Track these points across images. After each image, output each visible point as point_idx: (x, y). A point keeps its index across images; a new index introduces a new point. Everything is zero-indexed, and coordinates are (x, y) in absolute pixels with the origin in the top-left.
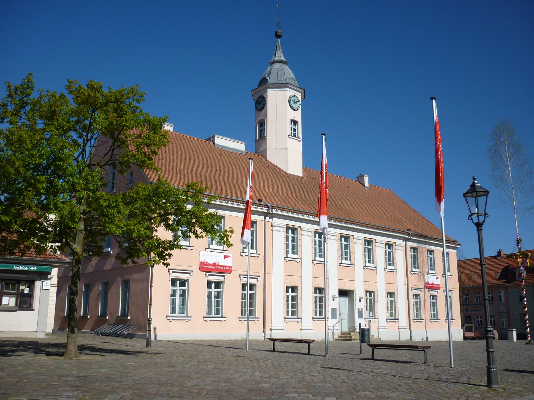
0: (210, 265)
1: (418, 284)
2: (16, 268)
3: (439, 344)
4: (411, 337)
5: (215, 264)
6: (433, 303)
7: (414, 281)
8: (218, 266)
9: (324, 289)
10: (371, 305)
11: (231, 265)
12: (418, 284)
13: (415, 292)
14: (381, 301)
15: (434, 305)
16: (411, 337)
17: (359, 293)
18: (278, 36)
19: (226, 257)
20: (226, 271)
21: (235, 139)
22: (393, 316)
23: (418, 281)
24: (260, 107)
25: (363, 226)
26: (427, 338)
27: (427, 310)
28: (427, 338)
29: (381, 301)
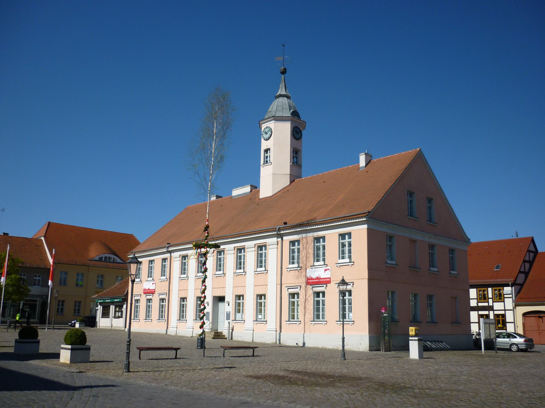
0: (314, 279)
1: (298, 281)
2: (116, 300)
3: (265, 346)
4: (343, 346)
5: (317, 278)
6: (163, 305)
7: (292, 278)
8: (320, 279)
9: (186, 298)
10: (239, 308)
11: (329, 276)
12: (298, 281)
13: (291, 291)
14: (250, 303)
15: (148, 307)
16: (343, 346)
17: (230, 298)
18: (284, 72)
19: (326, 270)
20: (327, 282)
21: (244, 185)
22: (182, 315)
23: (298, 277)
24: (298, 136)
25: (228, 238)
26: (304, 344)
27: (308, 311)
28: (304, 344)
29: (250, 303)
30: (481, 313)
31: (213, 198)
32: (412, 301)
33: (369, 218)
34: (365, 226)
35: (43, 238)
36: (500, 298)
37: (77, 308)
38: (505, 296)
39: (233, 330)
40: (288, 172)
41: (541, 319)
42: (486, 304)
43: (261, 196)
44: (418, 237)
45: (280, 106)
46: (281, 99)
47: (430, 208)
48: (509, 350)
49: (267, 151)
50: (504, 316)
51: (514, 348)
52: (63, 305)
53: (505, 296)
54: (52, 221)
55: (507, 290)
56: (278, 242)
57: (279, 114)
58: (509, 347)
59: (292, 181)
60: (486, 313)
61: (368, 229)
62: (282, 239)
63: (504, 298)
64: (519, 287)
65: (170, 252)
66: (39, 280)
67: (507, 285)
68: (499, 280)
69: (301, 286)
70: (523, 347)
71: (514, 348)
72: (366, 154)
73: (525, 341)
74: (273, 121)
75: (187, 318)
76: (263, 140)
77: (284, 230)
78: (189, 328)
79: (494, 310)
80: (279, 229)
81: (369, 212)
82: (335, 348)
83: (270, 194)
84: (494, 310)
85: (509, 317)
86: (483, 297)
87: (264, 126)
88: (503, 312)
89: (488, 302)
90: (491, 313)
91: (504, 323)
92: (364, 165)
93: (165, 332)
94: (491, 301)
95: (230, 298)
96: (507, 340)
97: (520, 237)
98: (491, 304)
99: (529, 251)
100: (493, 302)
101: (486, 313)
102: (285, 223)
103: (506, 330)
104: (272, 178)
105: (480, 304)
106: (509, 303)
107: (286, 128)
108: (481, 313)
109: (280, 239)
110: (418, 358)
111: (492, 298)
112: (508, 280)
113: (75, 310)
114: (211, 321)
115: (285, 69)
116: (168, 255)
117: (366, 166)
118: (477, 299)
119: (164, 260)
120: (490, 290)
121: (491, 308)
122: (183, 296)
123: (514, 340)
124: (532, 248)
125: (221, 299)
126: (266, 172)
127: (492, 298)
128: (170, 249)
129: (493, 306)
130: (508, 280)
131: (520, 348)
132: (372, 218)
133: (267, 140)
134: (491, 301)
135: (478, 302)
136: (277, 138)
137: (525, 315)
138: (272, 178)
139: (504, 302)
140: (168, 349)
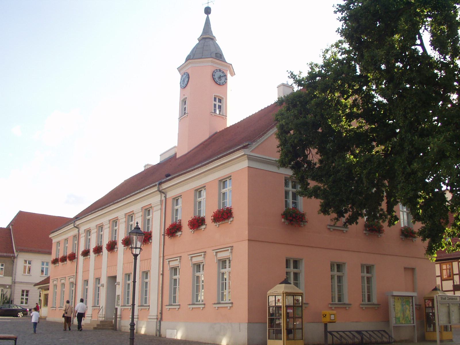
56: (161, 201)
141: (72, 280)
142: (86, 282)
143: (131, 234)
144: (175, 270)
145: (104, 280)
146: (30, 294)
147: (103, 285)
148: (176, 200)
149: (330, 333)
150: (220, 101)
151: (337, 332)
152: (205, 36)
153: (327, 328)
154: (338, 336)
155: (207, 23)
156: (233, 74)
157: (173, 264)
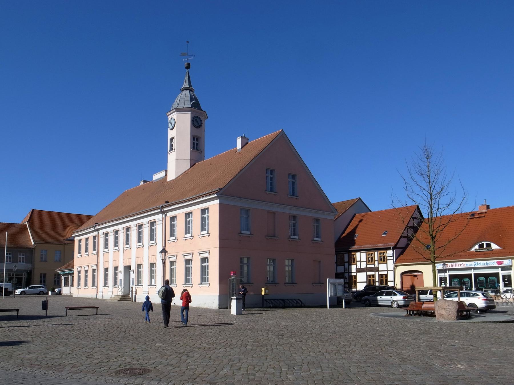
17: (134, 268)
30: (369, 273)
31: (142, 183)
32: (288, 266)
33: (221, 194)
34: (217, 202)
35: (27, 223)
36: (383, 260)
37: (43, 279)
38: (388, 258)
39: (136, 293)
40: (188, 157)
41: (416, 278)
42: (373, 266)
43: (168, 180)
44: (277, 209)
45: (184, 98)
46: (184, 92)
47: (293, 183)
48: (391, 306)
49: (172, 139)
50: (386, 276)
51: (395, 304)
52: (44, 277)
53: (388, 258)
54: (36, 208)
55: (390, 253)
56: (163, 218)
57: (181, 106)
58: (390, 304)
59: (191, 166)
60: (373, 273)
61: (220, 204)
62: (166, 215)
63: (387, 260)
64: (401, 250)
65: (98, 230)
66: (23, 258)
67: (389, 249)
68: (383, 245)
69: (177, 255)
70: (402, 303)
71: (395, 304)
72: (242, 137)
73: (404, 298)
74: (176, 113)
75: (143, 284)
76: (169, 130)
77: (165, 207)
78: (110, 293)
79: (378, 271)
80: (162, 207)
81: (220, 189)
82: (198, 306)
83: (174, 178)
84: (378, 271)
85: (390, 277)
86: (371, 260)
87: (170, 117)
88: (385, 273)
89: (374, 264)
90: (377, 273)
91: (387, 281)
92: (240, 147)
93: (95, 297)
94: (376, 263)
95: (134, 268)
96: (388, 298)
97: (408, 205)
98: (377, 266)
99: (414, 218)
100: (378, 264)
101: (373, 273)
102: (167, 202)
103: (357, 288)
104: (176, 164)
105: (368, 266)
106: (391, 264)
107: (187, 117)
108: (369, 273)
109: (164, 215)
110: (235, 314)
111: (378, 261)
112: (390, 244)
113: (55, 281)
114: (122, 287)
115: (189, 64)
116: (95, 233)
117: (242, 148)
118: (366, 261)
119: (95, 237)
120: (376, 253)
121: (376, 269)
122: (107, 267)
123: (395, 298)
124: (417, 215)
125: (129, 267)
126: (172, 157)
127: (378, 261)
128: (97, 228)
129: (378, 267)
130: (390, 244)
131: (400, 304)
132: (222, 194)
133: (172, 130)
134: (376, 263)
135: (367, 265)
136: (180, 127)
137: (403, 274)
138: (176, 164)
139: (387, 263)
140: (92, 308)
141: (94, 268)
142: (106, 269)
143: (445, 290)
144: (172, 263)
145: (121, 268)
146: (47, 276)
147: (121, 272)
148: (173, 219)
149: (266, 300)
150: (197, 140)
151: (270, 300)
152: (376, 245)
153: (27, 316)
154: (288, 302)
155: (358, 225)
156: (206, 117)
157: (172, 259)
